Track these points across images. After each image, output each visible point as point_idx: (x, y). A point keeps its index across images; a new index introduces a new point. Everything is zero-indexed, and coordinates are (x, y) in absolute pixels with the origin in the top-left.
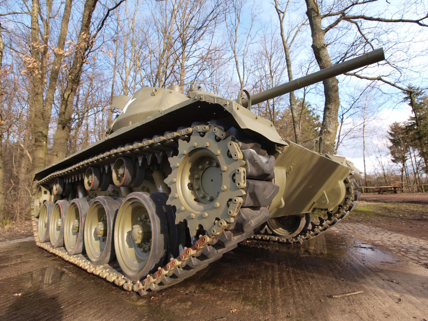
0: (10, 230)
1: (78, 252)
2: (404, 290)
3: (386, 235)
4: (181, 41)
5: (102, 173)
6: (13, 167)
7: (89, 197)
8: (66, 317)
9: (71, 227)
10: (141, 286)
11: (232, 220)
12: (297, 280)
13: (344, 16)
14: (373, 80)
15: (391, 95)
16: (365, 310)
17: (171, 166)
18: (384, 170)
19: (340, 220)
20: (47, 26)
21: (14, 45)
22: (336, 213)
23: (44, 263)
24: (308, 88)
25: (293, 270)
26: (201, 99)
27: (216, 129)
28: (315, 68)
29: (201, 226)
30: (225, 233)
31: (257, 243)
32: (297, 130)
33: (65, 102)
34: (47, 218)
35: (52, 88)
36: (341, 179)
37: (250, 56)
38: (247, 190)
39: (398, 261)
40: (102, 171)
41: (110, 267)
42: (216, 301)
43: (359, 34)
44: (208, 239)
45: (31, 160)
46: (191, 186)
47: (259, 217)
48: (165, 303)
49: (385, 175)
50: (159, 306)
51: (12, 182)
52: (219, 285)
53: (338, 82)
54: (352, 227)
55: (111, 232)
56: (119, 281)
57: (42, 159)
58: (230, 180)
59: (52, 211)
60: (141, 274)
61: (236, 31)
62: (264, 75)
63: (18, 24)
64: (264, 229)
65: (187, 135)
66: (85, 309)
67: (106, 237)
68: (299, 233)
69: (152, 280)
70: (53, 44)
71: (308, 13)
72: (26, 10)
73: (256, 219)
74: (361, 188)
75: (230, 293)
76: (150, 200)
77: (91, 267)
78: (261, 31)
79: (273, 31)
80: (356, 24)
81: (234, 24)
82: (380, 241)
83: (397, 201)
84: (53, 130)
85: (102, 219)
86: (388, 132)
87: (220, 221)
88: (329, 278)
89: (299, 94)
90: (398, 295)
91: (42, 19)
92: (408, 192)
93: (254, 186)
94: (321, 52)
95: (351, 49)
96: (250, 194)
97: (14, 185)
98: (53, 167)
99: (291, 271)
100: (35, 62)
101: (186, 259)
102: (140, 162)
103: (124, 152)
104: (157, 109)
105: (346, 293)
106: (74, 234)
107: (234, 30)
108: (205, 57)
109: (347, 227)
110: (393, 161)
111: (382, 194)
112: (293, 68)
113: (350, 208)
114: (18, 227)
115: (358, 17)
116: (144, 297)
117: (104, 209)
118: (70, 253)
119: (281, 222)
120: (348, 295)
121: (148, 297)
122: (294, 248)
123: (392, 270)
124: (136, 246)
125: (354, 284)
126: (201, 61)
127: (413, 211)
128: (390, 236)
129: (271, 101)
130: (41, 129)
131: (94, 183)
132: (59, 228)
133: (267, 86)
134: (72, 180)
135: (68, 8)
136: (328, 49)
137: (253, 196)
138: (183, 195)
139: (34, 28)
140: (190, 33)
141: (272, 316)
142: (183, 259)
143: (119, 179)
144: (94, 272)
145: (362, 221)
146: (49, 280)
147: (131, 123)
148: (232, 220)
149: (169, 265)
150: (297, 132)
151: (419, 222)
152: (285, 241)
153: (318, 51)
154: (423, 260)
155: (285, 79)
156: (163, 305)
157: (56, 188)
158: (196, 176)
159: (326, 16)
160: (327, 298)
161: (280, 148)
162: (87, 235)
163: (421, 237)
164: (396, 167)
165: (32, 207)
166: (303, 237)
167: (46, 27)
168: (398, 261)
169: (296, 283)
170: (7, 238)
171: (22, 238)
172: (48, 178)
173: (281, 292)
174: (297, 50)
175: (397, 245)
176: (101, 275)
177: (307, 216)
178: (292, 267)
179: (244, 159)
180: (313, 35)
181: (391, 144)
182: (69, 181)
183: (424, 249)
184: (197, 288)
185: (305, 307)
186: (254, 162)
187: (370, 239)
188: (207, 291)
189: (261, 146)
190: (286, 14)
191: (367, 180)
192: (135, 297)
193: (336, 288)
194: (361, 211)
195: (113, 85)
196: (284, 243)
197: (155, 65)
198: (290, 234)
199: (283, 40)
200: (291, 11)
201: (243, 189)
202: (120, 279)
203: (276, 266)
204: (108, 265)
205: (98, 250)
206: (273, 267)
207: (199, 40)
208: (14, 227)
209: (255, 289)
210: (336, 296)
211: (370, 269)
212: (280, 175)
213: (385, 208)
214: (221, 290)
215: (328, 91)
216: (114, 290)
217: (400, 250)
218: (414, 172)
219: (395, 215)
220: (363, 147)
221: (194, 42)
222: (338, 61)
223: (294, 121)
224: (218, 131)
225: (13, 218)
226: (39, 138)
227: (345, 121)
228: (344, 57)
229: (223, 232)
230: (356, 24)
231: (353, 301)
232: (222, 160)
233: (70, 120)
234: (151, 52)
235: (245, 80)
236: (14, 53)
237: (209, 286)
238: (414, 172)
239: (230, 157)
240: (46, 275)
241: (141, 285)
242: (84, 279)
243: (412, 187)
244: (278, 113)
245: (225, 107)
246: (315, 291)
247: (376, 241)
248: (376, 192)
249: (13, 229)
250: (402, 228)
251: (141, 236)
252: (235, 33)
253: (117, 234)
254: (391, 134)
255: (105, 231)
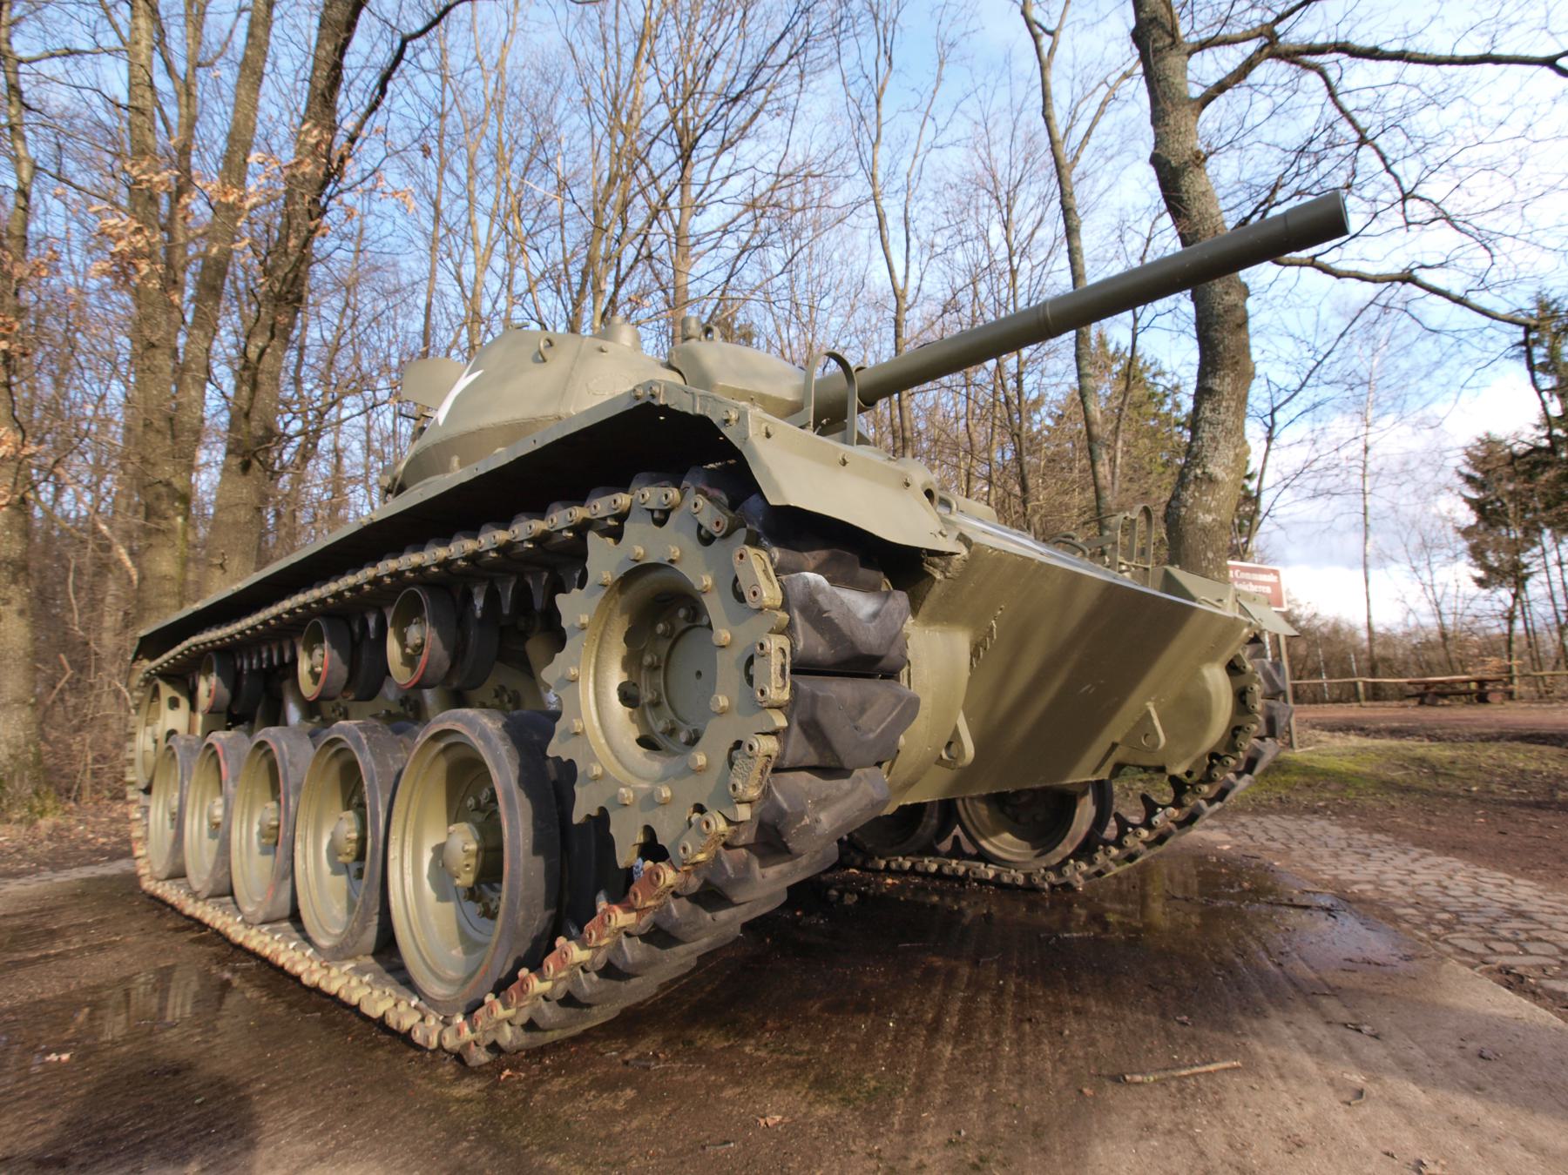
0: (57, 833)
1: (277, 915)
2: (1389, 1061)
3: (1401, 860)
4: (676, 142)
5: (357, 637)
6: (71, 610)
7: (323, 719)
8: (209, 1134)
9: (256, 828)
10: (467, 1034)
11: (744, 813)
12: (1021, 1021)
13: (1272, 47)
14: (1383, 281)
15: (1457, 335)
16: (1225, 1126)
17: (565, 624)
18: (1440, 614)
19: (1217, 805)
20: (189, 94)
21: (70, 166)
22: (1201, 782)
23: (163, 950)
24: (1147, 312)
25: (1018, 986)
26: (653, 396)
27: (701, 503)
28: (1168, 243)
29: (649, 831)
30: (726, 856)
31: (922, 888)
32: (1103, 470)
33: (249, 373)
34: (177, 795)
35: (207, 325)
36: (1211, 657)
37: (929, 195)
38: (792, 710)
39: (1407, 958)
40: (355, 629)
41: (378, 966)
42: (722, 1087)
43: (1332, 112)
44: (669, 876)
45: (135, 577)
46: (628, 696)
47: (849, 801)
48: (547, 1093)
49: (1444, 635)
50: (525, 1101)
51: (65, 662)
52: (745, 1034)
53: (1247, 295)
54: (1285, 830)
55: (380, 846)
56: (401, 1015)
57: (172, 579)
58: (738, 676)
59: (195, 770)
60: (469, 993)
61: (878, 102)
62: (985, 264)
63: (86, 93)
64: (951, 838)
65: (615, 517)
66: (273, 1108)
67: (365, 864)
68: (1069, 851)
69: (500, 1012)
70: (206, 166)
71: (1139, 36)
72: (110, 40)
73: (839, 807)
74: (1355, 684)
75: (778, 1061)
76: (504, 739)
77: (315, 965)
78: (973, 98)
79: (1019, 98)
80: (1322, 74)
81: (872, 75)
82: (1369, 882)
83: (1477, 735)
84: (209, 475)
85: (355, 800)
86: (1460, 474)
87: (706, 816)
88: (1141, 1016)
89: (1116, 330)
90: (1357, 1079)
91: (169, 69)
92: (1532, 700)
93: (814, 698)
94: (1185, 182)
95: (1294, 169)
96: (801, 724)
97: (70, 672)
98: (197, 615)
99: (1013, 988)
100: (139, 231)
101: (605, 941)
102: (479, 602)
103: (419, 569)
104: (550, 411)
105: (1179, 1067)
106: (264, 852)
107: (873, 99)
108: (764, 201)
109: (1265, 831)
110: (1481, 582)
111: (1433, 705)
112: (1088, 241)
113: (1251, 765)
114: (86, 825)
115: (1321, 50)
116: (477, 1072)
117: (356, 763)
118: (250, 919)
119: (1009, 810)
120: (1184, 1072)
121: (488, 1072)
122: (1053, 906)
123: (1374, 988)
124: (461, 894)
125: (1218, 1035)
126: (749, 216)
127: (1522, 771)
128: (1412, 867)
129: (1011, 362)
130: (166, 471)
131: (329, 672)
132: (215, 827)
133: (992, 305)
134: (260, 660)
135: (259, 32)
136: (1212, 165)
137: (813, 730)
138: (602, 725)
139: (137, 109)
140: (707, 111)
141: (898, 1139)
142: (593, 943)
143: (409, 661)
144: (323, 985)
145: (1326, 807)
146: (183, 1006)
147: (455, 460)
148: (744, 813)
149: (550, 963)
150: (1100, 476)
151: (1537, 812)
152: (1021, 880)
153: (1174, 176)
154: (1500, 954)
155: (1060, 281)
156: (538, 1097)
157: (207, 686)
158: (647, 660)
159: (1203, 46)
160: (1108, 1083)
161: (937, 560)
162: (305, 856)
163: (1526, 871)
164: (1488, 604)
165: (130, 756)
166: (1084, 866)
167: (184, 99)
168: (1407, 958)
169: (1016, 1029)
170: (46, 864)
171: (96, 863)
172: (181, 653)
173: (953, 1059)
174: (1109, 167)
175: (1426, 899)
176: (343, 995)
177: (1102, 792)
178: (1018, 976)
179: (785, 606)
180: (1157, 118)
181: (1468, 517)
182: (251, 664)
183: (1521, 915)
184: (667, 1042)
185: (1021, 1115)
186: (814, 612)
187: (1335, 876)
188: (701, 1054)
189: (856, 558)
190: (1064, 36)
191: (1378, 650)
192: (448, 1069)
193: (1150, 1051)
194: (1325, 773)
195: (429, 306)
196: (1018, 887)
197: (576, 232)
198: (1038, 856)
199: (1050, 134)
200: (1078, 26)
201: (779, 708)
202: (403, 1007)
203: (965, 971)
204: (370, 960)
205: (338, 909)
206: (951, 975)
207: (742, 137)
208: (72, 822)
209: (866, 1049)
210: (1138, 1078)
211: (1295, 985)
212: (937, 657)
213: (1421, 761)
214: (747, 1049)
215: (1210, 325)
216: (383, 1045)
217: (1430, 918)
218: (1558, 621)
219: (1453, 787)
220: (1361, 527)
221: (724, 147)
222: (1247, 213)
223: (1091, 437)
224: (704, 508)
225: (67, 792)
226: (158, 500)
227: (1284, 436)
228: (1269, 202)
229: (718, 854)
230: (1322, 74)
231: (1193, 1096)
232: (715, 606)
233: (273, 437)
234: (563, 185)
235: (913, 282)
236: (72, 194)
237: (711, 1037)
238: (1558, 621)
239: (740, 597)
240: (172, 993)
241: (467, 1029)
242: (291, 1006)
243: (1548, 680)
244: (1038, 403)
245: (723, 430)
246: (1073, 1057)
247: (1355, 883)
248: (1408, 697)
249: (69, 830)
250: (1469, 836)
251: (473, 861)
252: (873, 109)
253: (398, 854)
254: (1469, 479)
255: (362, 840)
